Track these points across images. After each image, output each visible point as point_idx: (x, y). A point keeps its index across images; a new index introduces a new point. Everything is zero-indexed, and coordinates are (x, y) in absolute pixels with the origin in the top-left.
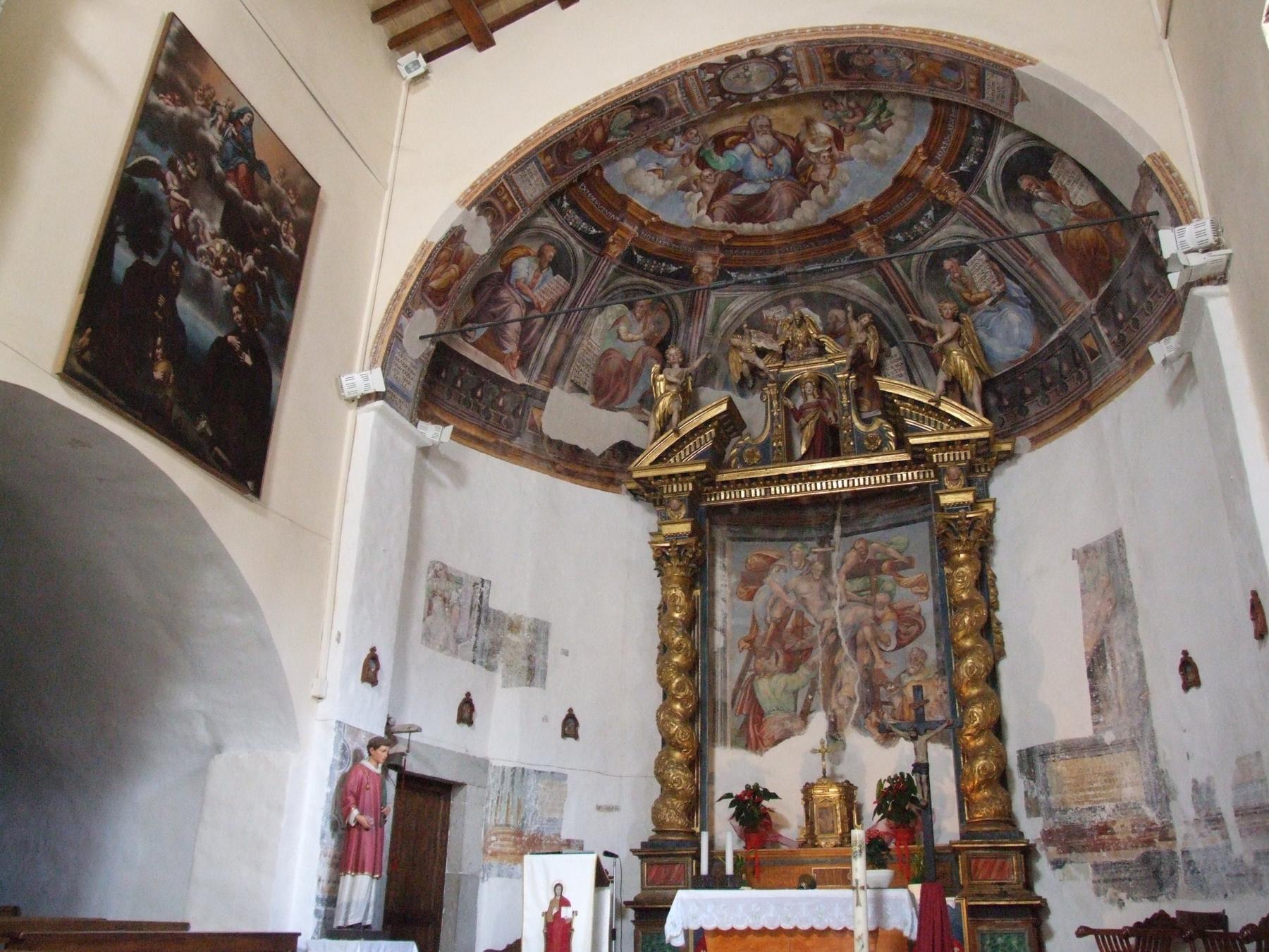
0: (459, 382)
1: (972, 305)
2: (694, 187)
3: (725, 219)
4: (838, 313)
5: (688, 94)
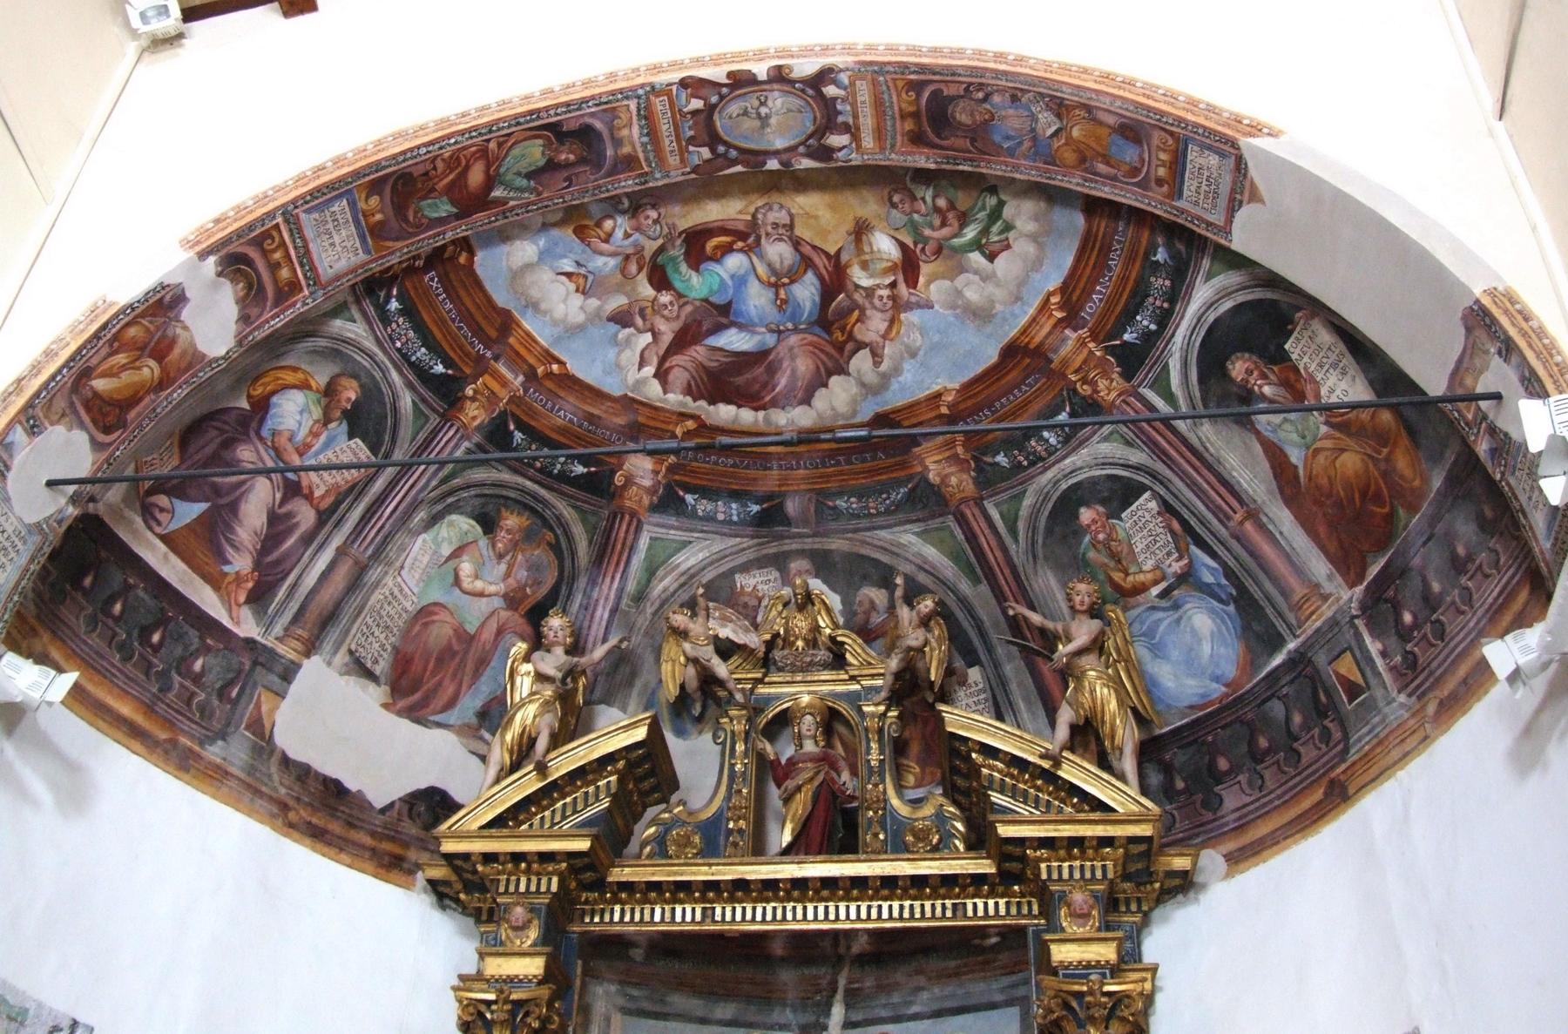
0: (118, 607)
1: (1128, 595)
2: (639, 321)
3: (688, 391)
4: (878, 596)
5: (652, 132)
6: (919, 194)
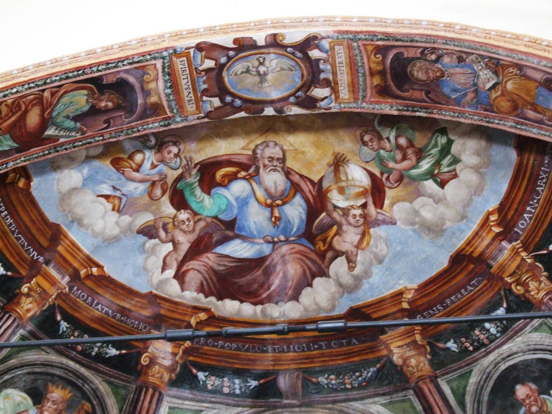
2: (162, 234)
3: (201, 289)
5: (174, 86)
6: (385, 134)
